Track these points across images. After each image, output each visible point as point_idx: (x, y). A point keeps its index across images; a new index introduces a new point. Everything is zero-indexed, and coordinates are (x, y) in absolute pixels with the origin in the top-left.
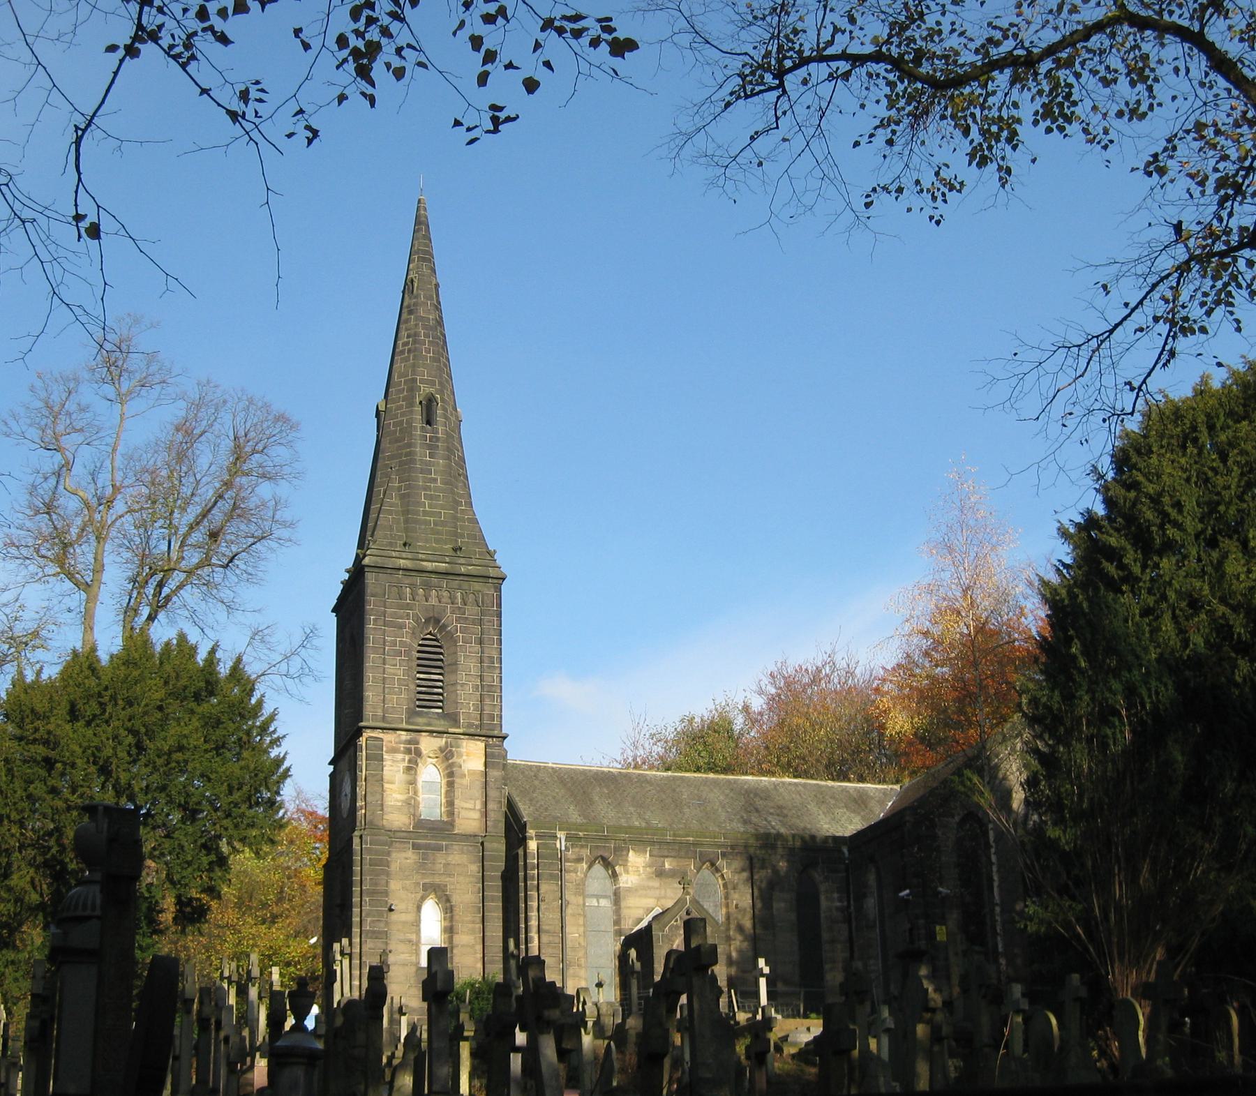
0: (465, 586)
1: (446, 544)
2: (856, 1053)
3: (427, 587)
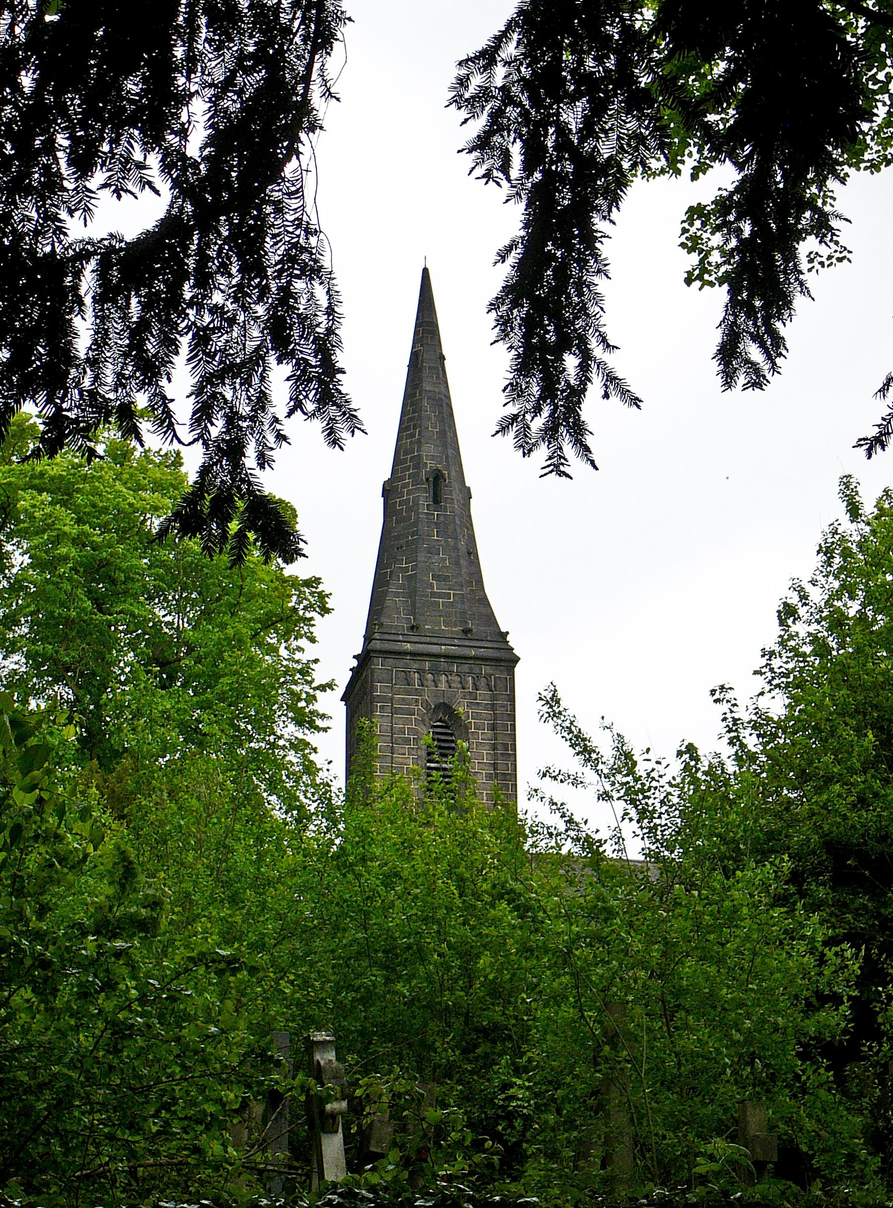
0: (476, 670)
1: (456, 626)
2: (537, 176)
3: (435, 672)
